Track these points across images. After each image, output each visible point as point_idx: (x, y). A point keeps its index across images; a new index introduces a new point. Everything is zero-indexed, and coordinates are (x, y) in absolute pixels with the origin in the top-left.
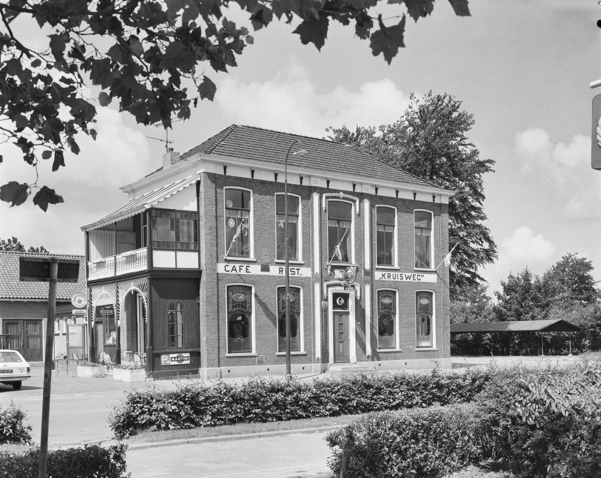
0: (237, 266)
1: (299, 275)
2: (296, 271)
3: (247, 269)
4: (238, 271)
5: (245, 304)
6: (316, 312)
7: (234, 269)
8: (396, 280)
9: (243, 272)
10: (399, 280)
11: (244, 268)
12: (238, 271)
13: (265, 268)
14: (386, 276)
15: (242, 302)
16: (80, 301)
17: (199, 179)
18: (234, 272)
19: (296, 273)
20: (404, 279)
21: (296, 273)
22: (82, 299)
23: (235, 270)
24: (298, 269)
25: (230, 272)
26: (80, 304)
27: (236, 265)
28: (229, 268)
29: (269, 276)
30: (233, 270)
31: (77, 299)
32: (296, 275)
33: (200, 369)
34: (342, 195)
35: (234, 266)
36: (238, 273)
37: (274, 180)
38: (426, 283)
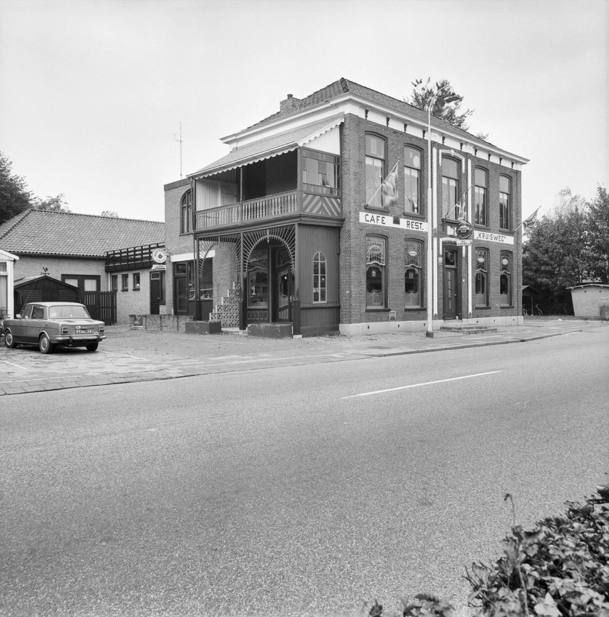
0: (375, 216)
1: (422, 230)
2: (419, 225)
3: (383, 220)
4: (376, 221)
5: (380, 257)
6: (469, 251)
7: (372, 220)
8: (488, 240)
9: (380, 223)
10: (490, 240)
11: (380, 219)
12: (376, 221)
13: (396, 221)
14: (481, 235)
15: (378, 255)
16: (160, 256)
17: (343, 121)
18: (372, 223)
19: (420, 228)
20: (493, 240)
21: (420, 228)
22: (162, 254)
23: (374, 220)
24: (421, 224)
25: (369, 223)
26: (160, 259)
27: (374, 215)
28: (369, 218)
29: (399, 229)
30: (371, 220)
31: (158, 254)
32: (419, 230)
33: (340, 325)
34: (452, 151)
35: (373, 216)
36: (376, 224)
37: (487, 159)
38: (507, 244)
